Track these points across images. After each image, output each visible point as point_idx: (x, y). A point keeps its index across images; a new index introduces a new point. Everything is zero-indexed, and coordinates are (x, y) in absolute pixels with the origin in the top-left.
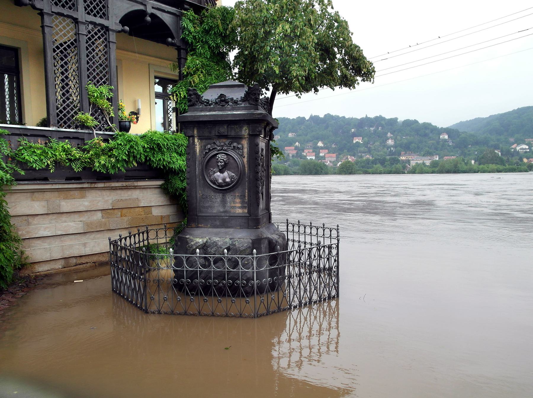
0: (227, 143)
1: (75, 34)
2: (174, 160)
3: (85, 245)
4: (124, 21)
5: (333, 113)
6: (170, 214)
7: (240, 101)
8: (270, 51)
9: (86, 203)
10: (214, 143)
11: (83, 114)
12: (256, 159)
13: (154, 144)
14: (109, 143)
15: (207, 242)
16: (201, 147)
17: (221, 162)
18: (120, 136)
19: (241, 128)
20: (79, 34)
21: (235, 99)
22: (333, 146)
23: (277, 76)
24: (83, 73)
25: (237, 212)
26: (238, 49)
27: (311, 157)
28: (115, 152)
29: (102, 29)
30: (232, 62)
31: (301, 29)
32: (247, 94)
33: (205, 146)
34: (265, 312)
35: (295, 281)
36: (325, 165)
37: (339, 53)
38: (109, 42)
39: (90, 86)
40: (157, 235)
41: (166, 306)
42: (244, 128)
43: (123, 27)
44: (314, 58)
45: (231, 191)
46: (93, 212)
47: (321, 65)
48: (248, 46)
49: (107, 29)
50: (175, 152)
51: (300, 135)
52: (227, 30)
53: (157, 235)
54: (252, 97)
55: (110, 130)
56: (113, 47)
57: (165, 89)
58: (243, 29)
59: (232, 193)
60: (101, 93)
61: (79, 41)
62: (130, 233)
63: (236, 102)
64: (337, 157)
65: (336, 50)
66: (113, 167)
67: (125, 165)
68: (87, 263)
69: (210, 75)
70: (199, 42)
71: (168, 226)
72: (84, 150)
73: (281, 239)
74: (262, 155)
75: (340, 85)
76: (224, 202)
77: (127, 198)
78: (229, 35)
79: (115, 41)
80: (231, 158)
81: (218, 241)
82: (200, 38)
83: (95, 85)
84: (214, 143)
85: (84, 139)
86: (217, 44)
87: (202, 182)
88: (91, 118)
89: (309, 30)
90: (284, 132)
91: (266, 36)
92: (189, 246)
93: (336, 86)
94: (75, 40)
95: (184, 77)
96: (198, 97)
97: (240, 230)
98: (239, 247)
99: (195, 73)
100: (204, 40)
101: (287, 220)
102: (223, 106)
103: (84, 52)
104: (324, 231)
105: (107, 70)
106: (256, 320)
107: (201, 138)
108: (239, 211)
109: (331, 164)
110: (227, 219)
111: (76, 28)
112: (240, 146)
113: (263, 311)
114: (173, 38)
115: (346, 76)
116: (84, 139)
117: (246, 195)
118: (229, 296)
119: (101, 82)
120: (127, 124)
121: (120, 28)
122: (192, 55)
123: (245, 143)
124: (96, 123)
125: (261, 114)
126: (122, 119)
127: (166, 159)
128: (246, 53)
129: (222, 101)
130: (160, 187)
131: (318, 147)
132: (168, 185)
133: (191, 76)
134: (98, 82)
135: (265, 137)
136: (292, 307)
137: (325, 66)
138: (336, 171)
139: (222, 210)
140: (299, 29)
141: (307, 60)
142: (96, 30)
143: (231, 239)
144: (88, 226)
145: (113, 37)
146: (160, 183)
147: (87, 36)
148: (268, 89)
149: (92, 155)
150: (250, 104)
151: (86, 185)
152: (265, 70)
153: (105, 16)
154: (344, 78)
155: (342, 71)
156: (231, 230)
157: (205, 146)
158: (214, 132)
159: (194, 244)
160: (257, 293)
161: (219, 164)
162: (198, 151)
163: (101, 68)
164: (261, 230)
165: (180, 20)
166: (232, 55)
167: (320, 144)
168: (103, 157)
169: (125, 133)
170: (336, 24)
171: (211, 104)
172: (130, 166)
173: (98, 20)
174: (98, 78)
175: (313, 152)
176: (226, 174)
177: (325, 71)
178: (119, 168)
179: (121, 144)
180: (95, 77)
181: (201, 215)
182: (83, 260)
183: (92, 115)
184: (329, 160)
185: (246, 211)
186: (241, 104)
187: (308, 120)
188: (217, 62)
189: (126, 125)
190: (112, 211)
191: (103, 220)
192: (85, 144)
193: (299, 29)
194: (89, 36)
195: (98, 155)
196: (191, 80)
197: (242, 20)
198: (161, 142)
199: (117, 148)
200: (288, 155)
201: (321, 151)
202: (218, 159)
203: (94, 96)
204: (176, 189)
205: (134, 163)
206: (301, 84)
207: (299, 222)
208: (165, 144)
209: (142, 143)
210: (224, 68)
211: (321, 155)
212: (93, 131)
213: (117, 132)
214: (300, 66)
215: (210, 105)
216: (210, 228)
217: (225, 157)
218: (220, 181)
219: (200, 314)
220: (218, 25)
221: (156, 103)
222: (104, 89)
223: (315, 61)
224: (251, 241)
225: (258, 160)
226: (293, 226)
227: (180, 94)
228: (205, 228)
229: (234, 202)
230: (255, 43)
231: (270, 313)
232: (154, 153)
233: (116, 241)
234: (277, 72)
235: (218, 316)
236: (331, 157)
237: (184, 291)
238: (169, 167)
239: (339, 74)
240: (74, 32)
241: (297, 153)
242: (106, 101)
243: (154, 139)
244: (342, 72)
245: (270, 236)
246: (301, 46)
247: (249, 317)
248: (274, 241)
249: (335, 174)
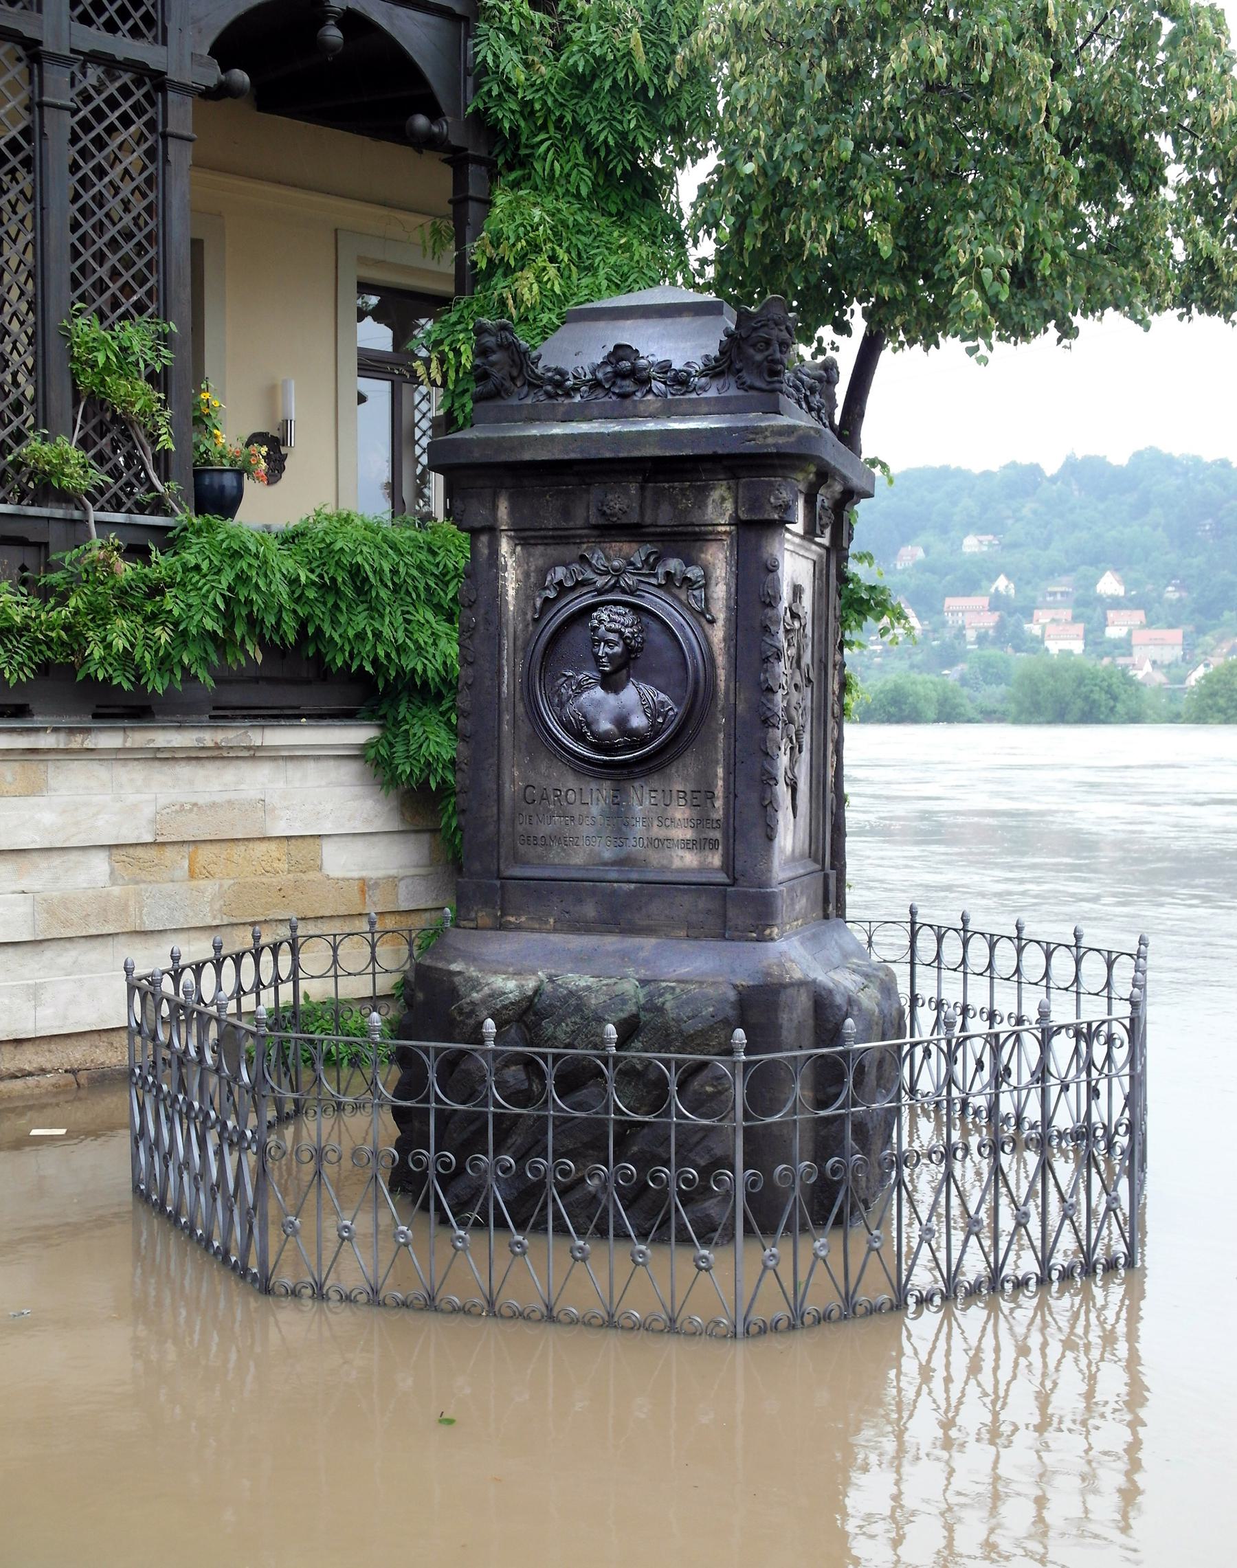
0: (638, 559)
1: (28, 108)
2: (423, 637)
3: (35, 993)
4: (227, 49)
5: (1177, 445)
6: (402, 872)
7: (702, 374)
8: (855, 159)
9: (48, 818)
10: (583, 559)
11: (45, 438)
12: (766, 629)
13: (343, 579)
14: (148, 563)
15: (537, 991)
16: (527, 575)
17: (607, 642)
18: (198, 532)
19: (702, 493)
20: (41, 105)
21: (678, 365)
22: (1171, 593)
23: (882, 269)
24: (53, 266)
25: (677, 863)
26: (720, 157)
27: (1064, 642)
28: (171, 603)
29: (139, 83)
30: (688, 212)
31: (998, 55)
32: (734, 346)
33: (543, 572)
34: (783, 1312)
35: (925, 1179)
36: (1129, 681)
37: (1178, 160)
38: (165, 136)
39: (80, 321)
40: (335, 961)
41: (352, 1272)
42: (716, 495)
43: (223, 71)
44: (1056, 181)
45: (647, 774)
46: (74, 857)
47: (1097, 216)
48: (757, 141)
49: (158, 82)
50: (428, 602)
51: (1015, 545)
52: (667, 71)
53: (335, 961)
54: (750, 360)
55: (158, 506)
56: (180, 155)
57: (402, 336)
58: (740, 66)
59: (655, 781)
60: (124, 349)
61: (43, 134)
62: (217, 948)
63: (681, 381)
64: (1189, 646)
65: (1165, 144)
66: (164, 663)
67: (214, 658)
68: (43, 1071)
69: (588, 269)
70: (544, 127)
71: (390, 923)
72: (45, 593)
73: (873, 991)
74: (795, 616)
75: (1183, 302)
76: (618, 819)
77: (218, 798)
78: (676, 95)
79: (187, 132)
80: (654, 625)
81: (588, 988)
82: (550, 111)
83: (102, 317)
84: (583, 559)
85: (46, 545)
86: (624, 135)
87: (525, 728)
88: (76, 455)
89: (1037, 57)
90: (944, 530)
91: (838, 93)
92: (460, 1011)
93: (1158, 309)
94: (26, 133)
95: (475, 282)
96: (521, 359)
97: (685, 945)
98: (678, 1021)
99: (523, 260)
100: (569, 118)
101: (913, 913)
102: (624, 396)
103: (61, 185)
104: (1078, 961)
105: (152, 252)
106: (740, 1351)
107: (524, 538)
108: (686, 860)
109: (1160, 677)
110: (631, 894)
111: (31, 82)
112: (694, 572)
113: (773, 1307)
114: (434, 113)
115: (1210, 261)
116: (46, 545)
117: (719, 790)
118: (622, 1235)
119: (127, 305)
120: (229, 480)
121: (211, 75)
122: (515, 185)
123: (718, 561)
124: (99, 476)
125: (791, 430)
126: (208, 462)
127: (387, 632)
128: (750, 168)
129: (620, 375)
130: (361, 754)
131: (1100, 599)
132: (391, 745)
133: (505, 275)
134: (115, 304)
135: (810, 533)
136: (911, 1301)
137: (1114, 222)
138: (1181, 708)
139: (608, 854)
140: (989, 56)
141: (1026, 193)
142: (112, 89)
143: (644, 982)
144: (51, 912)
145: (180, 115)
146: (359, 735)
147: (74, 112)
148: (843, 328)
149: (77, 612)
150: (742, 385)
151: (47, 741)
152: (832, 245)
153: (151, 26)
154: (1199, 271)
155: (1191, 241)
156: (648, 944)
157: (543, 572)
158: (584, 513)
159: (484, 1001)
160: (748, 1231)
161: (602, 650)
162: (511, 592)
163: (128, 248)
164: (780, 945)
165: (468, 36)
166: (689, 183)
167: (1109, 585)
168: (121, 623)
169: (214, 519)
170: (1167, 26)
171: (576, 389)
172: (236, 660)
173: (123, 46)
174: (114, 288)
175: (1075, 619)
176: (630, 694)
177: (1108, 247)
178: (185, 670)
179: (197, 568)
180: (100, 287)
181: (517, 872)
182: (28, 1059)
183: (84, 443)
184: (1151, 654)
185: (716, 860)
186: (704, 389)
187: (1053, 480)
188: (620, 214)
189: (222, 488)
190: (153, 853)
191: (116, 890)
192: (50, 568)
193: (989, 56)
194: (85, 112)
195: (99, 615)
196: (507, 294)
197: (736, 26)
198: (366, 558)
199: (182, 584)
200: (960, 634)
201: (1111, 614)
202: (595, 629)
203: (94, 365)
204: (428, 764)
205: (250, 647)
206: (993, 304)
207: (965, 921)
208: (387, 567)
209: (287, 563)
210: (652, 239)
211: (1114, 632)
212: (85, 510)
213: (184, 516)
214: (989, 218)
215: (568, 394)
216: (555, 930)
217: (628, 620)
218: (605, 725)
219: (492, 1308)
220: (629, 53)
221: (362, 399)
222: (136, 336)
223: (1056, 195)
224: (732, 995)
225: (773, 635)
226: (940, 939)
227: (458, 353)
228: (533, 930)
229: (663, 821)
230: (787, 125)
231: (808, 1319)
232: (336, 606)
233: (154, 982)
234: (886, 250)
235: (574, 1322)
236: (1161, 643)
237: (425, 1208)
238: (401, 672)
239: (1179, 251)
240: (23, 96)
241: (1000, 626)
242: (142, 383)
243: (337, 546)
244: (1195, 244)
245: (821, 976)
246: (999, 132)
247: (710, 1332)
248: (839, 1000)
249: (1175, 718)
